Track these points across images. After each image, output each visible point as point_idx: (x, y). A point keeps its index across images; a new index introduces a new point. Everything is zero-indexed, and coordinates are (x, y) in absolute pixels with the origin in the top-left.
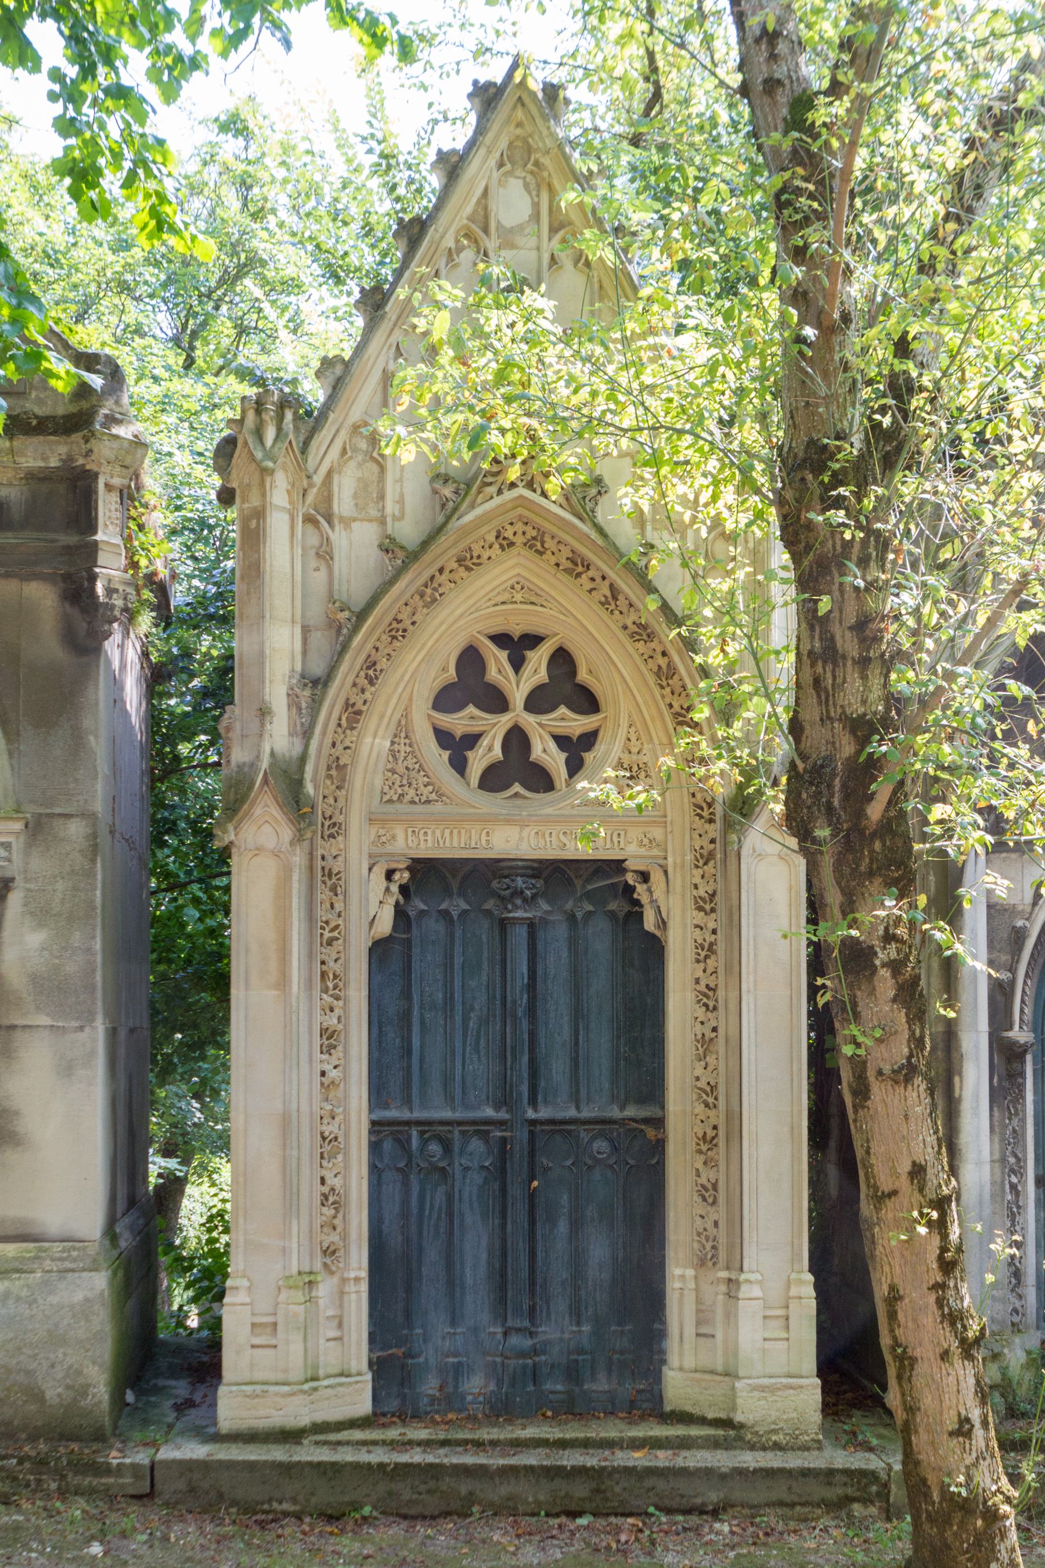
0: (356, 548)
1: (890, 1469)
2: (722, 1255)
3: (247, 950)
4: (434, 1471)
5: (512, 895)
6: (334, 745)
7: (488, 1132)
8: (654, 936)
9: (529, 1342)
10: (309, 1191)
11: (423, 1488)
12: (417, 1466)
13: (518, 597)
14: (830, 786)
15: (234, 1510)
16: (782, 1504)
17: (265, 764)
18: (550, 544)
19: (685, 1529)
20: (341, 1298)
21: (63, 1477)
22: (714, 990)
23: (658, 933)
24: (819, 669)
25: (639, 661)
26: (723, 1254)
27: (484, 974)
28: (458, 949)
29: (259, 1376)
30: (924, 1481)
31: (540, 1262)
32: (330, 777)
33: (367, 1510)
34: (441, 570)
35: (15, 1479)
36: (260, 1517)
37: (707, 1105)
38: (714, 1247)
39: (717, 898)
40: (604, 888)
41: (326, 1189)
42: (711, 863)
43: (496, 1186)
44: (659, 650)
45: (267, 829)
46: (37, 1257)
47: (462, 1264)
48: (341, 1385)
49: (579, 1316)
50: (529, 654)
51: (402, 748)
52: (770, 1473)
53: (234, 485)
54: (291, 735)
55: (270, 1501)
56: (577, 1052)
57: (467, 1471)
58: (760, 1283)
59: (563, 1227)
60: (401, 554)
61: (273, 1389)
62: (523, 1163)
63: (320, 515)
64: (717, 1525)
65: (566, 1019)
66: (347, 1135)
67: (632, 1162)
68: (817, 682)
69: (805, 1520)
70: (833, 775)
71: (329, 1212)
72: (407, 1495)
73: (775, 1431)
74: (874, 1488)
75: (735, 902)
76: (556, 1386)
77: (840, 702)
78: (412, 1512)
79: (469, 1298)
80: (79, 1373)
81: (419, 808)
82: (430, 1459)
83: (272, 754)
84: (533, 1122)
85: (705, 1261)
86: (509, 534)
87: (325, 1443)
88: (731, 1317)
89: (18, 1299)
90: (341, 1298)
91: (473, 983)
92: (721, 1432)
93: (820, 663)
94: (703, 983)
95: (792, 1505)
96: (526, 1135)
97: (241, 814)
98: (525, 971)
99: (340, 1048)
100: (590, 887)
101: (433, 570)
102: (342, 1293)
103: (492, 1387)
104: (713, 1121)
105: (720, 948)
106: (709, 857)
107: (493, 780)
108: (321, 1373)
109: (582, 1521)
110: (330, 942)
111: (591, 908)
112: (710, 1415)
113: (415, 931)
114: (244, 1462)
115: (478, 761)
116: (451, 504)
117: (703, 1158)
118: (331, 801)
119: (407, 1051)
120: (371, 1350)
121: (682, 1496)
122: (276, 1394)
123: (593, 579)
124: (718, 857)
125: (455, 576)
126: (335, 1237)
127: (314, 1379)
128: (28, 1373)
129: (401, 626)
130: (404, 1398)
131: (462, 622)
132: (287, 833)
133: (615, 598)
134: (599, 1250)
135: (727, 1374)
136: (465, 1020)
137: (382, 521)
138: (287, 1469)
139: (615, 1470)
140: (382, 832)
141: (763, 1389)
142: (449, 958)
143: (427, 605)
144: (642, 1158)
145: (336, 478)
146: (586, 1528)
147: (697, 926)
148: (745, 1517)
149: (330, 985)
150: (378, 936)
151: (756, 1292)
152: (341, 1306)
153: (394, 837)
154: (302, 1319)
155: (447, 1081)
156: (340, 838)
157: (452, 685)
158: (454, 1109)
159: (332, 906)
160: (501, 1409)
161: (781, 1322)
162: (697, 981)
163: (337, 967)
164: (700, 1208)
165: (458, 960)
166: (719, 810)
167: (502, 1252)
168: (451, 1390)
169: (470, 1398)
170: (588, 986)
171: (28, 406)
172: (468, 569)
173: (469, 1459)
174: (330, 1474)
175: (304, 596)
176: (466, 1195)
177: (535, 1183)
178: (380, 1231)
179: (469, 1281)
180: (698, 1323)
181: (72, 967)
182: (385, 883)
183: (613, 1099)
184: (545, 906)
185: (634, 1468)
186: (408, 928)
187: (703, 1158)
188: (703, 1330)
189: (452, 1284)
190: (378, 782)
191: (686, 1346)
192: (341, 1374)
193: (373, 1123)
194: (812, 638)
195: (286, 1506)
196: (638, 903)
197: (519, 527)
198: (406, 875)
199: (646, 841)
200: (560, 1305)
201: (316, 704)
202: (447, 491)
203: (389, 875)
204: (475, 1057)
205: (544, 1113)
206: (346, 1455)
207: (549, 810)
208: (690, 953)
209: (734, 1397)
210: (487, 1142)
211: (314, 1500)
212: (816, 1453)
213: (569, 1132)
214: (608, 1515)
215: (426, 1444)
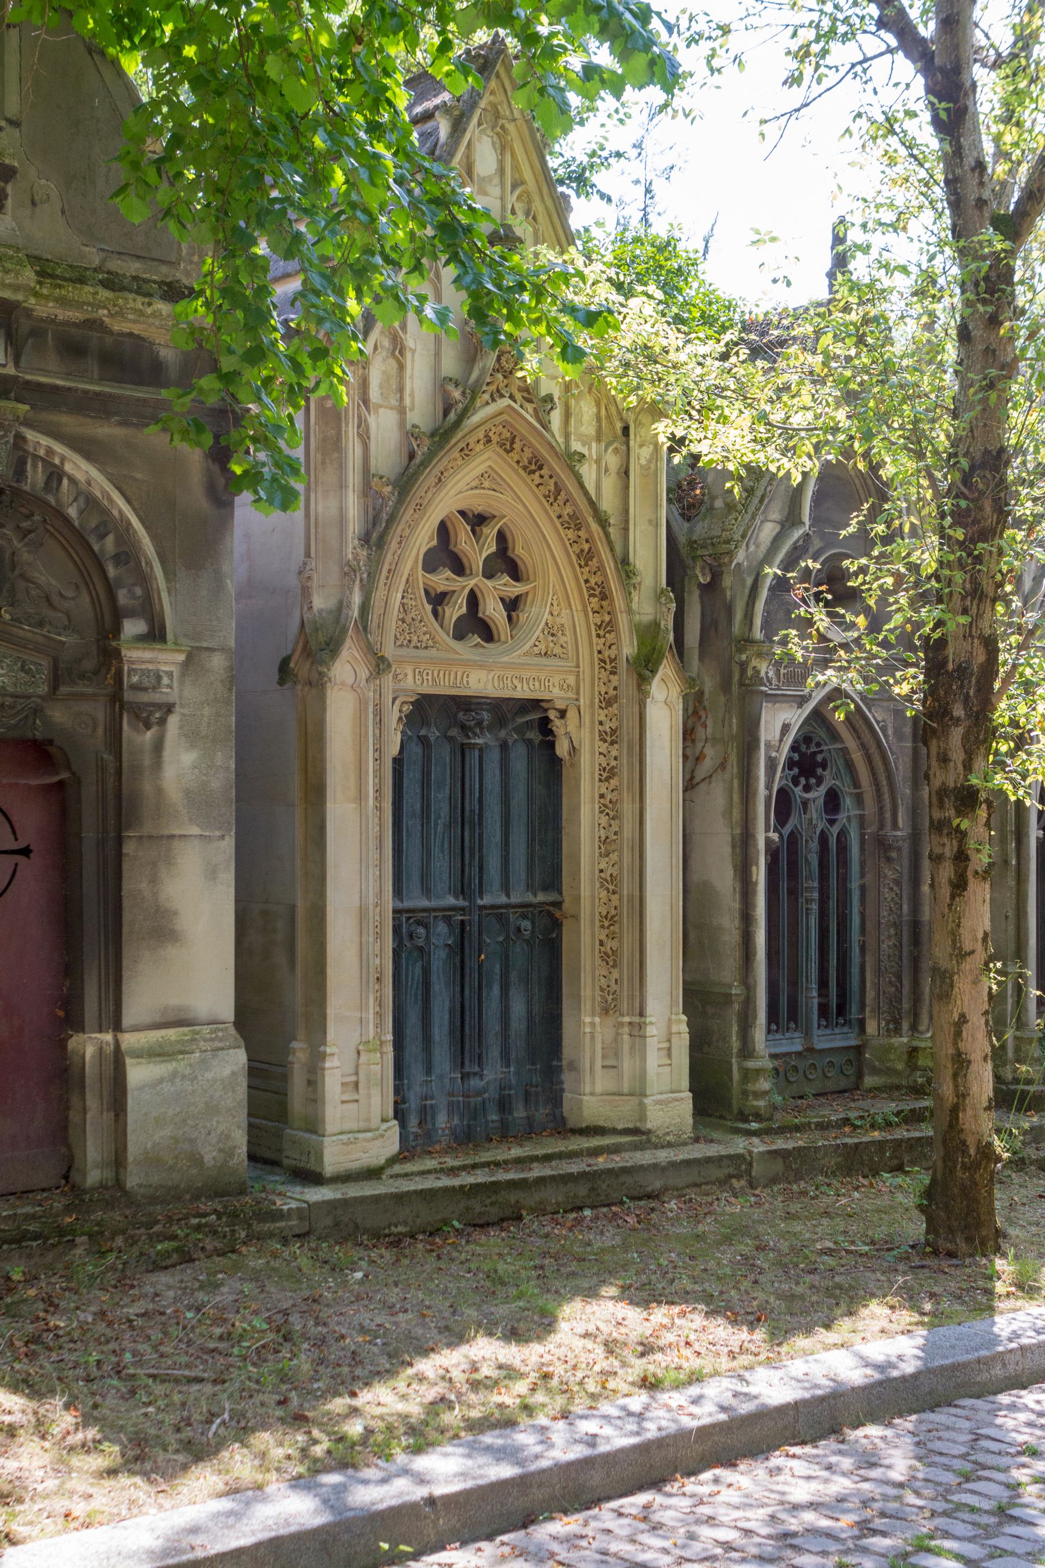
16: (696, 1185)
21: (250, 1226)
24: (968, 603)
26: (626, 1001)
30: (964, 1143)
35: (215, 1232)
40: (532, 724)
46: (193, 1040)
57: (513, 1184)
59: (496, 990)
61: (361, 1136)
72: (478, 1209)
80: (228, 1137)
89: (183, 1077)
112: (620, 1127)
128: (192, 1141)
144: (548, 933)
158: (429, 899)
171: (178, 275)
181: (215, 784)
195: (401, 1229)
200: (494, 1052)
207: (506, 659)
211: (418, 1221)
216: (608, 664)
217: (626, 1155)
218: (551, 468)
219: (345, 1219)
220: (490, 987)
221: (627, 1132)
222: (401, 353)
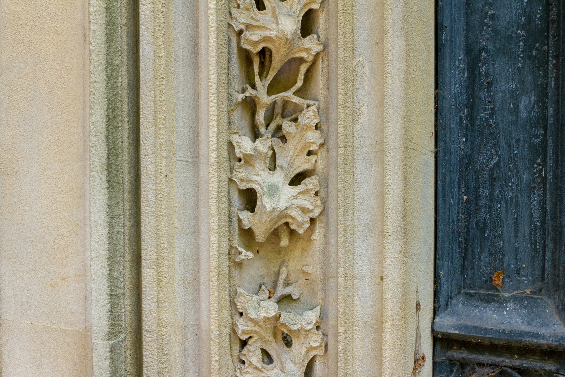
75: (441, 144)
193: (441, 341)
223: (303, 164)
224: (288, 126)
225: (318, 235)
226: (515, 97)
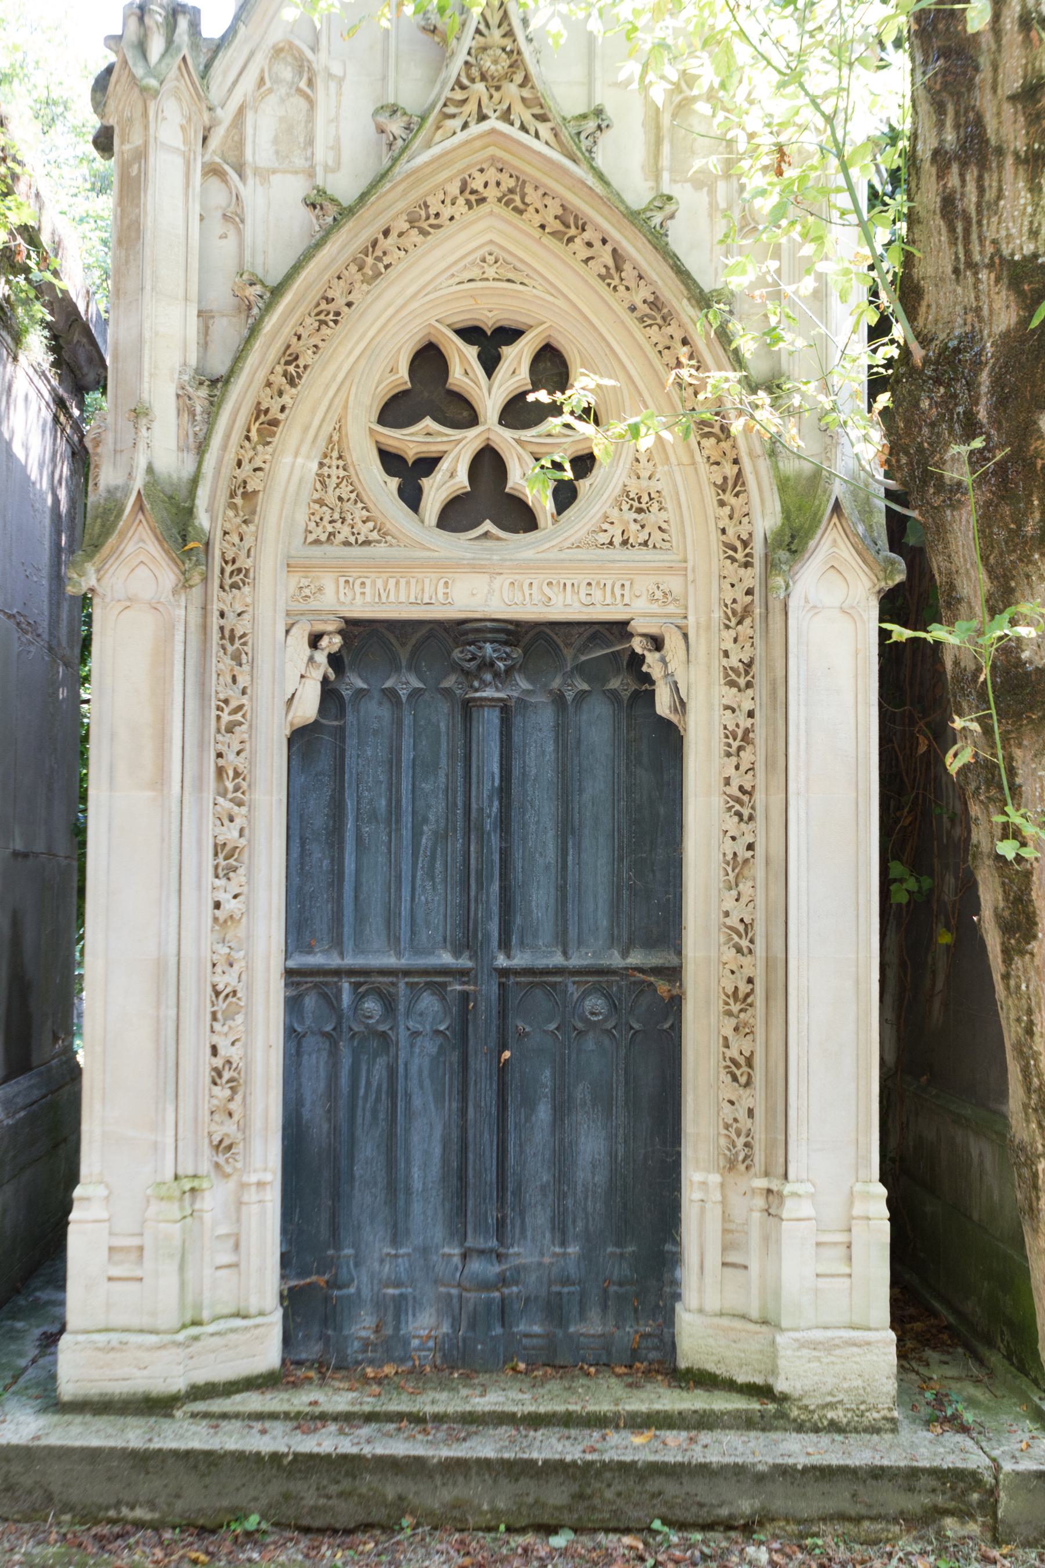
0: (275, 213)
1: (998, 1468)
2: (759, 1157)
3: (113, 736)
4: (348, 1465)
5: (479, 668)
6: (239, 464)
7: (444, 985)
8: (669, 723)
9: (496, 1269)
10: (196, 1065)
11: (333, 1489)
12: (324, 1460)
13: (491, 272)
14: (971, 385)
15: (67, 1517)
16: (842, 1517)
17: (139, 482)
18: (532, 197)
19: (705, 1557)
20: (238, 1210)
22: (750, 794)
23: (674, 718)
24: (953, 180)
25: (652, 354)
26: (760, 1154)
27: (442, 773)
28: (407, 741)
29: (120, 1319)
31: (511, 1160)
32: (233, 506)
33: (253, 1521)
34: (386, 233)
36: (105, 1530)
37: (739, 950)
38: (747, 1145)
39: (756, 668)
41: (218, 1062)
42: (747, 622)
43: (455, 1057)
44: (678, 336)
45: (142, 572)
47: (408, 1162)
48: (233, 1330)
49: (563, 1232)
50: (505, 350)
51: (334, 472)
52: (825, 1473)
53: (112, 121)
54: (180, 449)
55: (117, 1505)
56: (564, 879)
58: (812, 1196)
59: (543, 1113)
60: (332, 210)
62: (490, 1026)
63: (226, 166)
64: (751, 1550)
65: (551, 834)
66: (249, 988)
67: (636, 1026)
68: (948, 204)
69: (876, 1542)
70: (978, 364)
71: (222, 1093)
72: (310, 1499)
73: (832, 1406)
74: (975, 1496)
75: (780, 673)
76: (532, 1327)
77: (990, 234)
78: (317, 1523)
79: (417, 1207)
81: (356, 551)
82: (346, 1447)
83: (150, 470)
84: (505, 972)
85: (737, 1160)
86: (477, 184)
87: (206, 1415)
88: (770, 1242)
90: (238, 1210)
91: (427, 787)
92: (756, 1406)
93: (955, 168)
94: (735, 784)
95: (858, 1520)
96: (495, 988)
97: (105, 550)
98: (496, 770)
99: (241, 871)
100: (583, 658)
101: (373, 230)
102: (240, 1204)
103: (446, 1328)
104: (747, 972)
105: (759, 736)
106: (744, 615)
107: (455, 516)
108: (206, 1315)
109: (559, 1541)
110: (230, 730)
111: (585, 687)
112: (741, 1379)
113: (350, 717)
114: (83, 1450)
115: (438, 489)
116: (400, 143)
117: (733, 1022)
118: (236, 539)
119: (339, 876)
120: (283, 1277)
121: (701, 1505)
122: (140, 1347)
123: (589, 245)
124: (756, 612)
125: (404, 242)
126: (230, 1128)
127: (195, 1323)
129: (332, 307)
130: (327, 1340)
131: (415, 305)
132: (169, 576)
133: (619, 269)
134: (591, 1144)
135: (765, 1322)
136: (417, 834)
137: (311, 174)
138: (142, 1460)
139: (606, 1466)
140: (304, 582)
141: (815, 1345)
142: (395, 751)
143: (368, 281)
145: (250, 117)
146: (563, 1553)
147: (727, 707)
148: (790, 1536)
149: (230, 786)
150: (299, 722)
151: (806, 1209)
152: (238, 1220)
153: (320, 589)
154: (177, 1242)
155: (390, 918)
156: (246, 589)
157: (405, 393)
158: (399, 954)
159: (234, 679)
160: (459, 1361)
161: (842, 1251)
162: (727, 782)
163: (240, 762)
164: (730, 1091)
165: (407, 756)
166: (758, 548)
167: (460, 1147)
168: (389, 1331)
169: (415, 1343)
170: (581, 791)
172: (424, 233)
173: (399, 1447)
174: (202, 1467)
175: (201, 269)
176: (414, 1069)
177: (507, 1054)
178: (299, 1116)
179: (417, 1185)
180: (725, 1249)
182: (307, 651)
183: (613, 940)
184: (524, 685)
185: (634, 1463)
186: (341, 713)
187: (733, 1022)
188: (731, 1258)
189: (395, 1188)
190: (301, 517)
191: (708, 1279)
192: (237, 1315)
193: (289, 973)
194: (940, 125)
195: (139, 1513)
196: (648, 679)
197: (492, 175)
198: (338, 640)
199: (659, 594)
200: (539, 1217)
201: (214, 405)
202: (396, 127)
203: (315, 641)
204: (429, 885)
205: (520, 960)
206: (231, 1440)
207: (529, 554)
208: (718, 745)
209: (774, 1356)
210: (443, 999)
211: (179, 1505)
212: (888, 1436)
213: (554, 985)
214: (595, 1531)
215: (347, 1419)
216: (736, 551)
217: (614, 1438)
218: (597, 228)
219: (28, 1481)
220: (529, 1104)
221: (752, 1390)
222: (310, 83)
223: (237, 891)
224: (232, 875)
225: (244, 920)
226: (1025, 205)
